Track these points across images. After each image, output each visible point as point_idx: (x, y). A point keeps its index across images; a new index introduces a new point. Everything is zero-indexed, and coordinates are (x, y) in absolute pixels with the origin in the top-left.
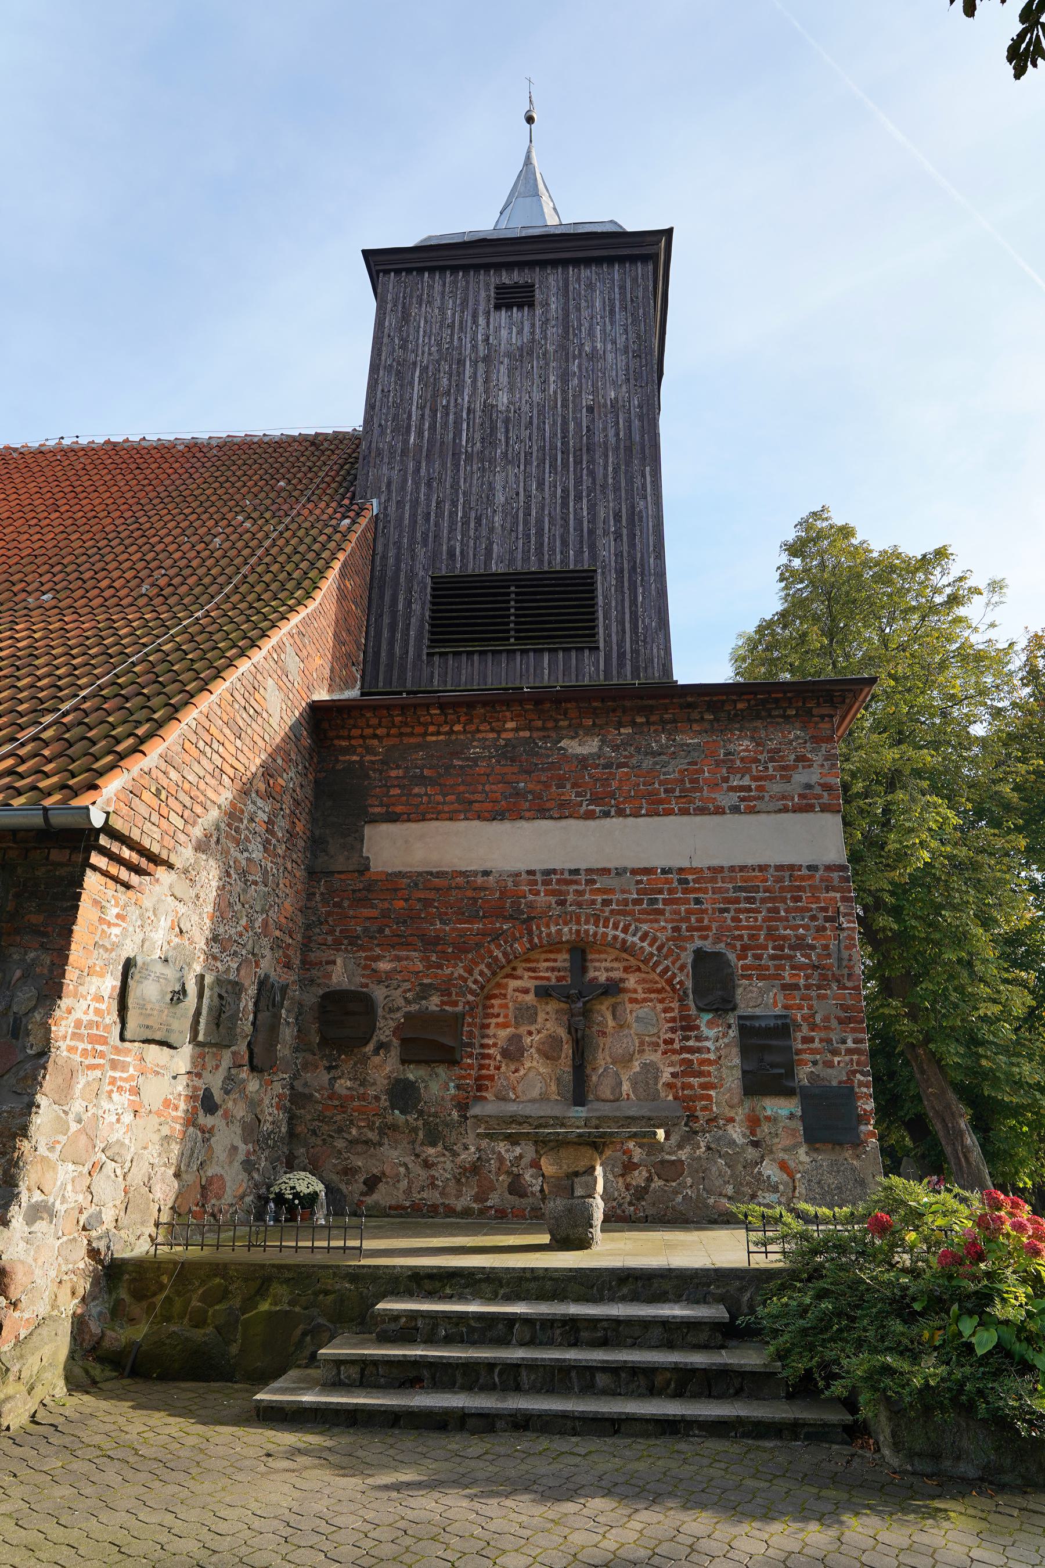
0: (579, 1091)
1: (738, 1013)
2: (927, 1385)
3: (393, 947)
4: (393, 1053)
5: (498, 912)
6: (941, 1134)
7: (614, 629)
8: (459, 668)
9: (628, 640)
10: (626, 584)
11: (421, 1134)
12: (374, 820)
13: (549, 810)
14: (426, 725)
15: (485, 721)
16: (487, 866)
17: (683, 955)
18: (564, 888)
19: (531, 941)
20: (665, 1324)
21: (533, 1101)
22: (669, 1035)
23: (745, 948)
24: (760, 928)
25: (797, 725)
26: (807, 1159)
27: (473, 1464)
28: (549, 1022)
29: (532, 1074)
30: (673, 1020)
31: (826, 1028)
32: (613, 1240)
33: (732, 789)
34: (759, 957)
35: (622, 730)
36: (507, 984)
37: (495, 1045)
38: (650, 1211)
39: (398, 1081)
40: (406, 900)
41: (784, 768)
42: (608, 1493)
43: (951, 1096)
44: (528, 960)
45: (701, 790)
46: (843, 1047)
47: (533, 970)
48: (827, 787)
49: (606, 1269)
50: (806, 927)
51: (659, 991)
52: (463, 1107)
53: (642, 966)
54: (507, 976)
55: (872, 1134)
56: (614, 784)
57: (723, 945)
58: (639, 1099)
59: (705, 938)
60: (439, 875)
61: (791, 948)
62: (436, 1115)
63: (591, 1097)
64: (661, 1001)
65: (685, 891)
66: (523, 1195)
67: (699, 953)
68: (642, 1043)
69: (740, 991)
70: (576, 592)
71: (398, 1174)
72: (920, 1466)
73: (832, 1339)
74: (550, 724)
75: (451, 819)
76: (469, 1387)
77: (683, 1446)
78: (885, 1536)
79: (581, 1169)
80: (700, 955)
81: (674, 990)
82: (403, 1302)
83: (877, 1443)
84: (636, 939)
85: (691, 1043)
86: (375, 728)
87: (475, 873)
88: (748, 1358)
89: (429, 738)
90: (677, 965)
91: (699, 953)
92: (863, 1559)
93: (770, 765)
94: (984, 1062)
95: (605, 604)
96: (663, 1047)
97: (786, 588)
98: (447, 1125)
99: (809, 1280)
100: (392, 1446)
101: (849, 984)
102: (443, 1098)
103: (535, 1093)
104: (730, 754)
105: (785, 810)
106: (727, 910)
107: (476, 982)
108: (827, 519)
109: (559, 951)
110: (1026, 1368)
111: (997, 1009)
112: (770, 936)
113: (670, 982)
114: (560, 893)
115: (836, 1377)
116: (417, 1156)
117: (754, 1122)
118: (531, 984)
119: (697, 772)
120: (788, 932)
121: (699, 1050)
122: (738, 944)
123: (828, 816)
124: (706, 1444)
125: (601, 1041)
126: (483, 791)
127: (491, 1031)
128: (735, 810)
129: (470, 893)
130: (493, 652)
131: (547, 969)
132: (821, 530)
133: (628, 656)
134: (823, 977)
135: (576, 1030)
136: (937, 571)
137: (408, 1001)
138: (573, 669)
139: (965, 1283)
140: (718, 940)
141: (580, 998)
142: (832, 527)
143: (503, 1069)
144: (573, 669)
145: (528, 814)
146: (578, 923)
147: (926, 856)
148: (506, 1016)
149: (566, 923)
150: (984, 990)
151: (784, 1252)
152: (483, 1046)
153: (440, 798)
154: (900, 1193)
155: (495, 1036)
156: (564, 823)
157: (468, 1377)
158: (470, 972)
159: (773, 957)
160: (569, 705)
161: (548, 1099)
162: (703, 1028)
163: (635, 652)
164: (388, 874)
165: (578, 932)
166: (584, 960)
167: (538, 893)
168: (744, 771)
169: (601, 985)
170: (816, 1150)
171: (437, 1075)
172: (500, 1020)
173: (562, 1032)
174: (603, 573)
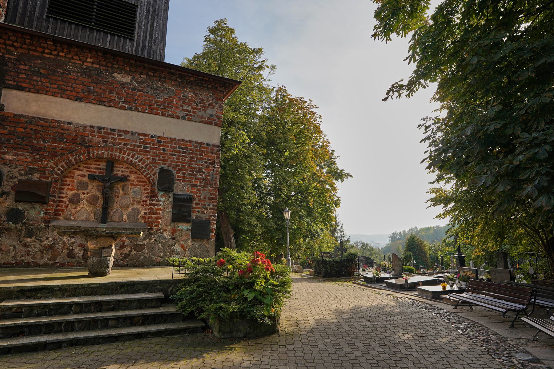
0: (104, 217)
1: (173, 193)
2: (233, 311)
3: (15, 149)
4: (11, 197)
5: (74, 141)
6: (225, 239)
7: (142, 34)
8: (64, 28)
9: (147, 41)
10: (150, 17)
11: (23, 233)
12: (8, 87)
13: (104, 102)
14: (44, 48)
15: (77, 55)
16: (71, 120)
17: (155, 169)
18: (107, 136)
19: (89, 156)
20: (139, 300)
21: (82, 221)
22: (146, 199)
23: (180, 170)
24: (186, 163)
25: (211, 92)
26: (191, 244)
27: (51, 362)
28: (93, 189)
29: (82, 210)
30: (148, 193)
31: (204, 200)
32: (115, 273)
33: (184, 110)
34: (184, 174)
35: (142, 76)
36: (75, 172)
37: (66, 197)
38: (130, 262)
39: (12, 209)
40: (24, 129)
41: (204, 107)
42: (116, 363)
43: (230, 227)
44: (86, 164)
45: (172, 108)
46: (209, 207)
47: (88, 168)
48: (218, 117)
49: (116, 283)
50: (203, 165)
51: (143, 182)
52: (47, 222)
53: (138, 172)
54: (75, 169)
55: (214, 236)
56: (135, 98)
57: (171, 168)
58: (129, 222)
59: (165, 164)
60: (44, 120)
61: (196, 172)
62: (32, 225)
63: (109, 220)
64: (144, 186)
65: (160, 145)
66: (74, 257)
67: (162, 170)
68: (134, 201)
69: (175, 185)
70: (126, 12)
71: (9, 250)
72: (226, 336)
73: (202, 300)
74: (109, 65)
75: (53, 96)
76: (48, 333)
77: (144, 342)
78: (218, 358)
79: (106, 246)
80: (162, 170)
81: (150, 182)
82: (14, 302)
83: (212, 331)
84: (137, 161)
85: (154, 202)
86: (13, 42)
87: (64, 122)
88: (170, 309)
89: (45, 55)
90: (153, 173)
91: (162, 170)
92: (212, 367)
93: (199, 104)
94: (241, 218)
95: (140, 22)
96: (142, 203)
97: (207, 44)
98: (38, 229)
99: (194, 282)
100: (7, 362)
101: (214, 186)
102: (37, 218)
103: (84, 218)
104: (185, 96)
105: (202, 122)
106: (175, 155)
107: (59, 170)
108: (225, 24)
109: (101, 161)
110: (261, 303)
111: (248, 201)
112: (189, 167)
113: (148, 179)
114: (105, 137)
115: (203, 312)
116: (21, 242)
117: (174, 231)
118: (86, 174)
119: (171, 100)
120: (196, 166)
121: (157, 205)
122: (177, 168)
123: (216, 127)
124: (153, 340)
125: (116, 199)
126: (72, 87)
127: (65, 191)
128: (184, 118)
129: (60, 131)
130: (83, 26)
131: (95, 168)
132: (222, 27)
133: (147, 47)
134: (206, 183)
135: (106, 194)
136: (257, 56)
137: (21, 175)
138: (121, 46)
139: (246, 280)
140: (170, 165)
141: (109, 182)
142: (227, 27)
143: (69, 207)
144: (121, 46)
145: (93, 101)
146: (112, 151)
147: (237, 150)
148: (73, 186)
149: (106, 150)
150: (246, 195)
151: (186, 273)
152: (60, 197)
153: (48, 85)
154: (228, 253)
155: (66, 193)
156: (110, 109)
157: (50, 328)
158: (57, 165)
159: (189, 174)
160: (119, 59)
161: (89, 220)
162: (160, 197)
163: (150, 47)
164: (14, 115)
165: (111, 155)
166: (113, 167)
167: (94, 136)
168: (189, 105)
169: (119, 177)
170: (195, 241)
171: (35, 208)
172: (70, 187)
173: (99, 194)
174: (141, 8)
